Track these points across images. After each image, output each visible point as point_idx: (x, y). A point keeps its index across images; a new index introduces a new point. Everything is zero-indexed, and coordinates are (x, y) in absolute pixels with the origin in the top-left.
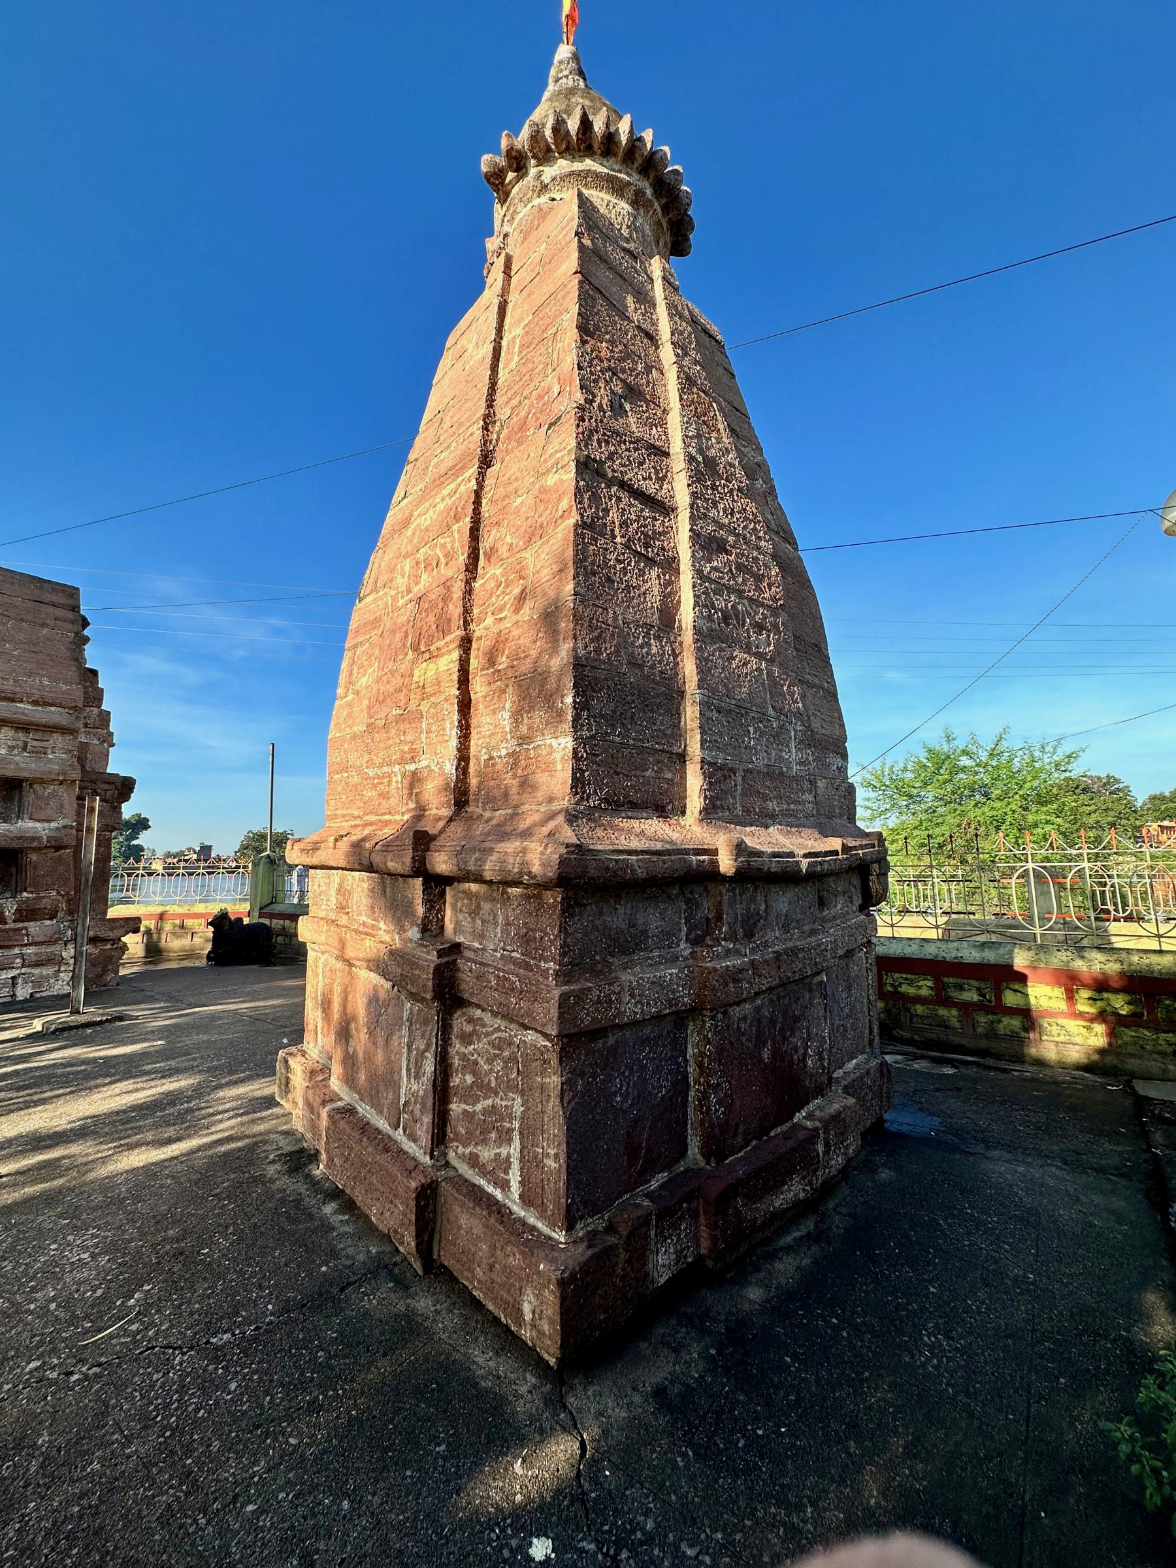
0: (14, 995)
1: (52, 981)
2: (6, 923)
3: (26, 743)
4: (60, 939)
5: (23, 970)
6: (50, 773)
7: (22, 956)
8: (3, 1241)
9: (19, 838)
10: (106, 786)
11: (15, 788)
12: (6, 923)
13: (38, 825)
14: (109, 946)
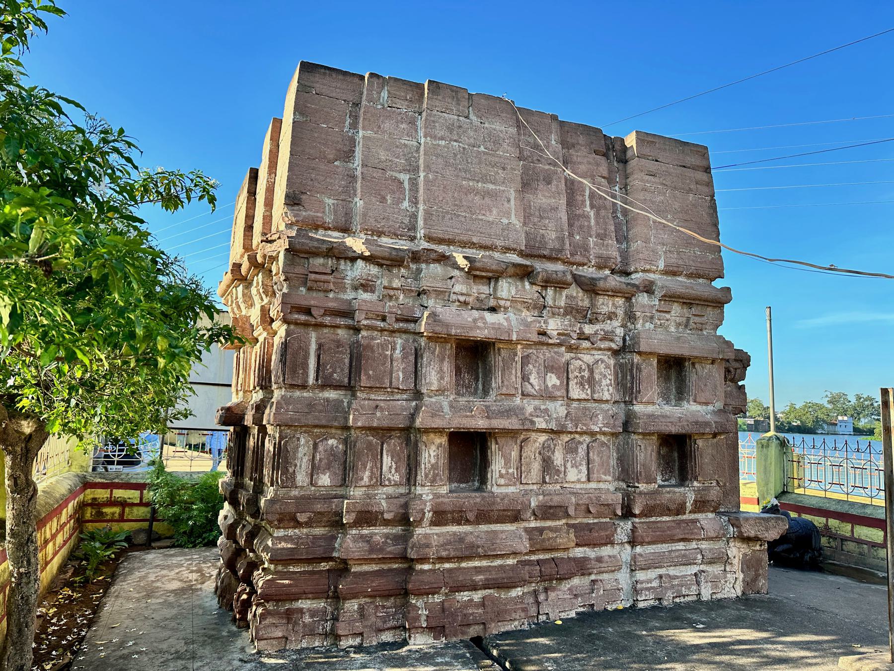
1: (722, 582)
3: (688, 319)
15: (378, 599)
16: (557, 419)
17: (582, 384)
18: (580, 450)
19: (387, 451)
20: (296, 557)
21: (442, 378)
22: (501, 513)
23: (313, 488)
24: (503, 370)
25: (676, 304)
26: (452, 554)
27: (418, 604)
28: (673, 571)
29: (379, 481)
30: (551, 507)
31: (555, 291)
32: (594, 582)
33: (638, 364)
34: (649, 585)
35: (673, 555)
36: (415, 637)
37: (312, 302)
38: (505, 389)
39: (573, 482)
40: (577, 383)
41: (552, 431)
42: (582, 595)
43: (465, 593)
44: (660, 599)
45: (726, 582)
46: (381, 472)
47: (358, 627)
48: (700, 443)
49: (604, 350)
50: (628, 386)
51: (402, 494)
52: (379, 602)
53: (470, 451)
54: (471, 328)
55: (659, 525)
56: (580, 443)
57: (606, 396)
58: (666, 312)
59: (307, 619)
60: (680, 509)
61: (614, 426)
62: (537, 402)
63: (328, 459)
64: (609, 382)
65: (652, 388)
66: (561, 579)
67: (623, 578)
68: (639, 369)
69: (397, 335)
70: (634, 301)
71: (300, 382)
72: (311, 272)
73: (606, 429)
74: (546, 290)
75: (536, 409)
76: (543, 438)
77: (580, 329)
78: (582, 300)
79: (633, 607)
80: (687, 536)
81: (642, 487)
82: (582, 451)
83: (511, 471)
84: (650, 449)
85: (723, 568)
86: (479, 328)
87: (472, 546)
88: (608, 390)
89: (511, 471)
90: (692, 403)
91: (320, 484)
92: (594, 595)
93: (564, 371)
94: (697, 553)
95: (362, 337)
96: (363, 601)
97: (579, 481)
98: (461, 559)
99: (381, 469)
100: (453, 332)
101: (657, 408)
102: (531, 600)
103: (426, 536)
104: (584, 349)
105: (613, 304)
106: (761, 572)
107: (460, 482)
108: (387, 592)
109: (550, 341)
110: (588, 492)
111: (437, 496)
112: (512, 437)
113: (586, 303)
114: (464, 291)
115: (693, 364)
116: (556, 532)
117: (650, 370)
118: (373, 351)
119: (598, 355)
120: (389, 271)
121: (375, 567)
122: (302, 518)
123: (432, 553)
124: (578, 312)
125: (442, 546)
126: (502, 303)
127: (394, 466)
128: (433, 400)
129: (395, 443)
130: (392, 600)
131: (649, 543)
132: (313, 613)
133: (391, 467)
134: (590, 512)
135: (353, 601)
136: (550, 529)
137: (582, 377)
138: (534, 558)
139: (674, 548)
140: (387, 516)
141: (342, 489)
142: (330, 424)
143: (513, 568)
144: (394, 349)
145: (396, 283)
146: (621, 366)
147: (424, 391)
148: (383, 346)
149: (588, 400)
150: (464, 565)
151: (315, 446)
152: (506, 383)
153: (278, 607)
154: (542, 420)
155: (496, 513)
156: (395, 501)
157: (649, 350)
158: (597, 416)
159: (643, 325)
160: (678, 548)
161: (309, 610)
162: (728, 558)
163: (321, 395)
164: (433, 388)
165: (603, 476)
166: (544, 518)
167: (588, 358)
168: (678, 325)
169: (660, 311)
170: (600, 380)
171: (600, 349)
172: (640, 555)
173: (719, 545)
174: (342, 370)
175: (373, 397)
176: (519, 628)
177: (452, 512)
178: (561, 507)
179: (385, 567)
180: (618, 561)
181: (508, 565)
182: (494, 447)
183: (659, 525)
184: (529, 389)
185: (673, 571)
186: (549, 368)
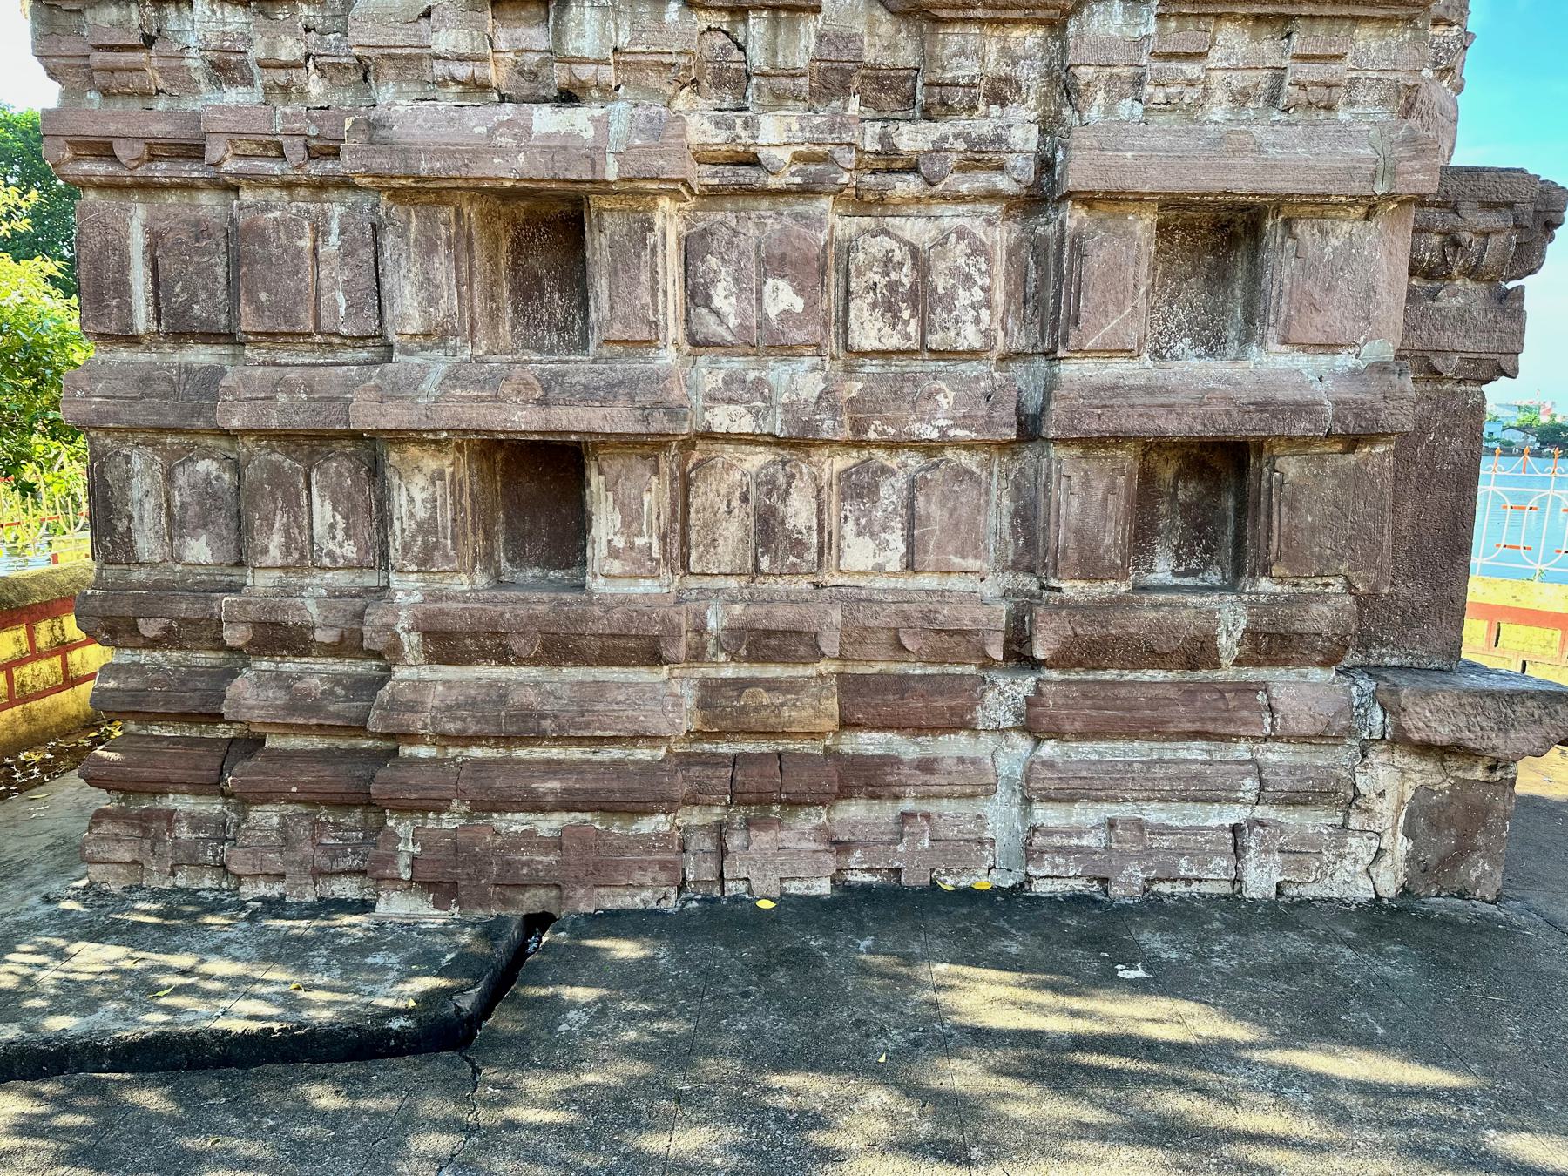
0: (1237, 881)
1: (1328, 856)
2: (1217, 665)
3: (1278, 74)
4: (1350, 731)
5: (1260, 812)
6: (1351, 172)
7: (1259, 770)
8: (5, 915)
9: (1262, 406)
10: (1490, 220)
11: (1232, 241)
12: (1217, 665)
13: (1302, 360)
14: (1479, 773)
15: (324, 810)
16: (789, 408)
17: (890, 309)
18: (884, 491)
19: (322, 489)
20: (144, 708)
21: (433, 301)
22: (609, 643)
23: (179, 568)
24: (614, 273)
25: (1229, 27)
26: (473, 729)
27: (400, 830)
28: (1154, 814)
29: (304, 557)
30: (769, 633)
31: (775, 23)
32: (906, 816)
33: (1078, 234)
34: (1074, 842)
35: (1158, 771)
36: (388, 898)
37: (112, 128)
38: (618, 326)
39: (864, 573)
40: (874, 305)
41: (774, 441)
42: (865, 846)
43: (518, 816)
44: (1104, 881)
45: (1342, 857)
46: (312, 537)
47: (273, 862)
48: (1290, 467)
49: (977, 198)
50: (1049, 300)
51: (367, 590)
52: (325, 816)
53: (539, 483)
54: (476, 154)
55: (1123, 692)
56: (885, 471)
57: (970, 337)
58: (1188, 57)
59: (184, 833)
60: (1199, 653)
61: (989, 423)
62: (737, 363)
63: (201, 504)
64: (979, 295)
65: (1120, 306)
66: (795, 804)
67: (1000, 816)
68: (1079, 251)
69: (334, 194)
70: (1071, 30)
71: (114, 328)
72: (98, 48)
73: (960, 433)
74: (745, 22)
75: (728, 382)
76: (757, 460)
77: (883, 137)
78: (892, 47)
79: (1019, 888)
80: (1210, 727)
81: (1073, 588)
82: (890, 492)
83: (640, 542)
84: (1099, 487)
85: (1338, 820)
86: (500, 151)
87: (527, 713)
88: (977, 321)
89: (640, 542)
90: (1274, 347)
91: (188, 559)
92: (901, 848)
93: (821, 270)
94: (1244, 775)
95: (240, 208)
96: (291, 809)
97: (879, 570)
98: (508, 740)
99: (311, 528)
100: (424, 168)
101: (1148, 363)
102: (708, 845)
103: (419, 685)
104: (905, 202)
105: (1004, 51)
106: (1480, 840)
107: (549, 564)
108: (338, 798)
109: (773, 183)
110: (904, 597)
111: (432, 596)
112: (644, 458)
113: (907, 55)
114: (465, 49)
115: (1288, 223)
116: (785, 692)
117: (1125, 253)
118: (264, 241)
119: (951, 217)
120: (267, 16)
121: (318, 743)
122: (150, 628)
123: (419, 722)
124: (882, 88)
125: (449, 708)
126: (585, 73)
127: (341, 524)
128: (416, 360)
129: (339, 468)
130: (358, 814)
131: (1083, 736)
132: (197, 823)
133: (332, 526)
134: (904, 648)
135: (267, 807)
136: (772, 685)
137: (893, 286)
138: (725, 748)
139: (1168, 755)
140: (321, 636)
141: (236, 571)
142: (186, 424)
143: (648, 769)
144: (320, 232)
145: (290, 49)
146: (1038, 247)
147: (394, 339)
148: (290, 227)
149: (914, 352)
150: (521, 753)
151: (169, 476)
152: (621, 309)
153: (128, 803)
154: (742, 409)
155: (596, 644)
156: (340, 603)
157: (1099, 185)
158: (931, 396)
159: (1109, 109)
160: (1183, 754)
161: (190, 816)
162: (1357, 795)
163: (177, 358)
164: (409, 330)
165: (956, 560)
166: (757, 655)
167: (915, 229)
168: (1241, 97)
169: (1168, 57)
170: (951, 295)
171: (959, 199)
172: (1049, 764)
173: (1338, 758)
174: (212, 295)
175: (283, 357)
176: (653, 905)
177: (475, 635)
178: (799, 633)
179: (343, 744)
180: (983, 772)
181: (636, 762)
182: (596, 481)
183: (1123, 692)
184: (709, 326)
185: (1154, 814)
186: (775, 264)
